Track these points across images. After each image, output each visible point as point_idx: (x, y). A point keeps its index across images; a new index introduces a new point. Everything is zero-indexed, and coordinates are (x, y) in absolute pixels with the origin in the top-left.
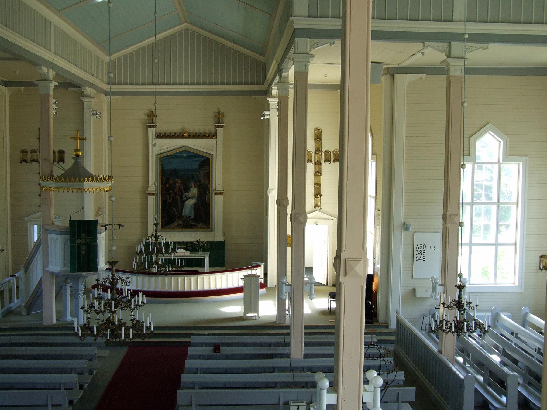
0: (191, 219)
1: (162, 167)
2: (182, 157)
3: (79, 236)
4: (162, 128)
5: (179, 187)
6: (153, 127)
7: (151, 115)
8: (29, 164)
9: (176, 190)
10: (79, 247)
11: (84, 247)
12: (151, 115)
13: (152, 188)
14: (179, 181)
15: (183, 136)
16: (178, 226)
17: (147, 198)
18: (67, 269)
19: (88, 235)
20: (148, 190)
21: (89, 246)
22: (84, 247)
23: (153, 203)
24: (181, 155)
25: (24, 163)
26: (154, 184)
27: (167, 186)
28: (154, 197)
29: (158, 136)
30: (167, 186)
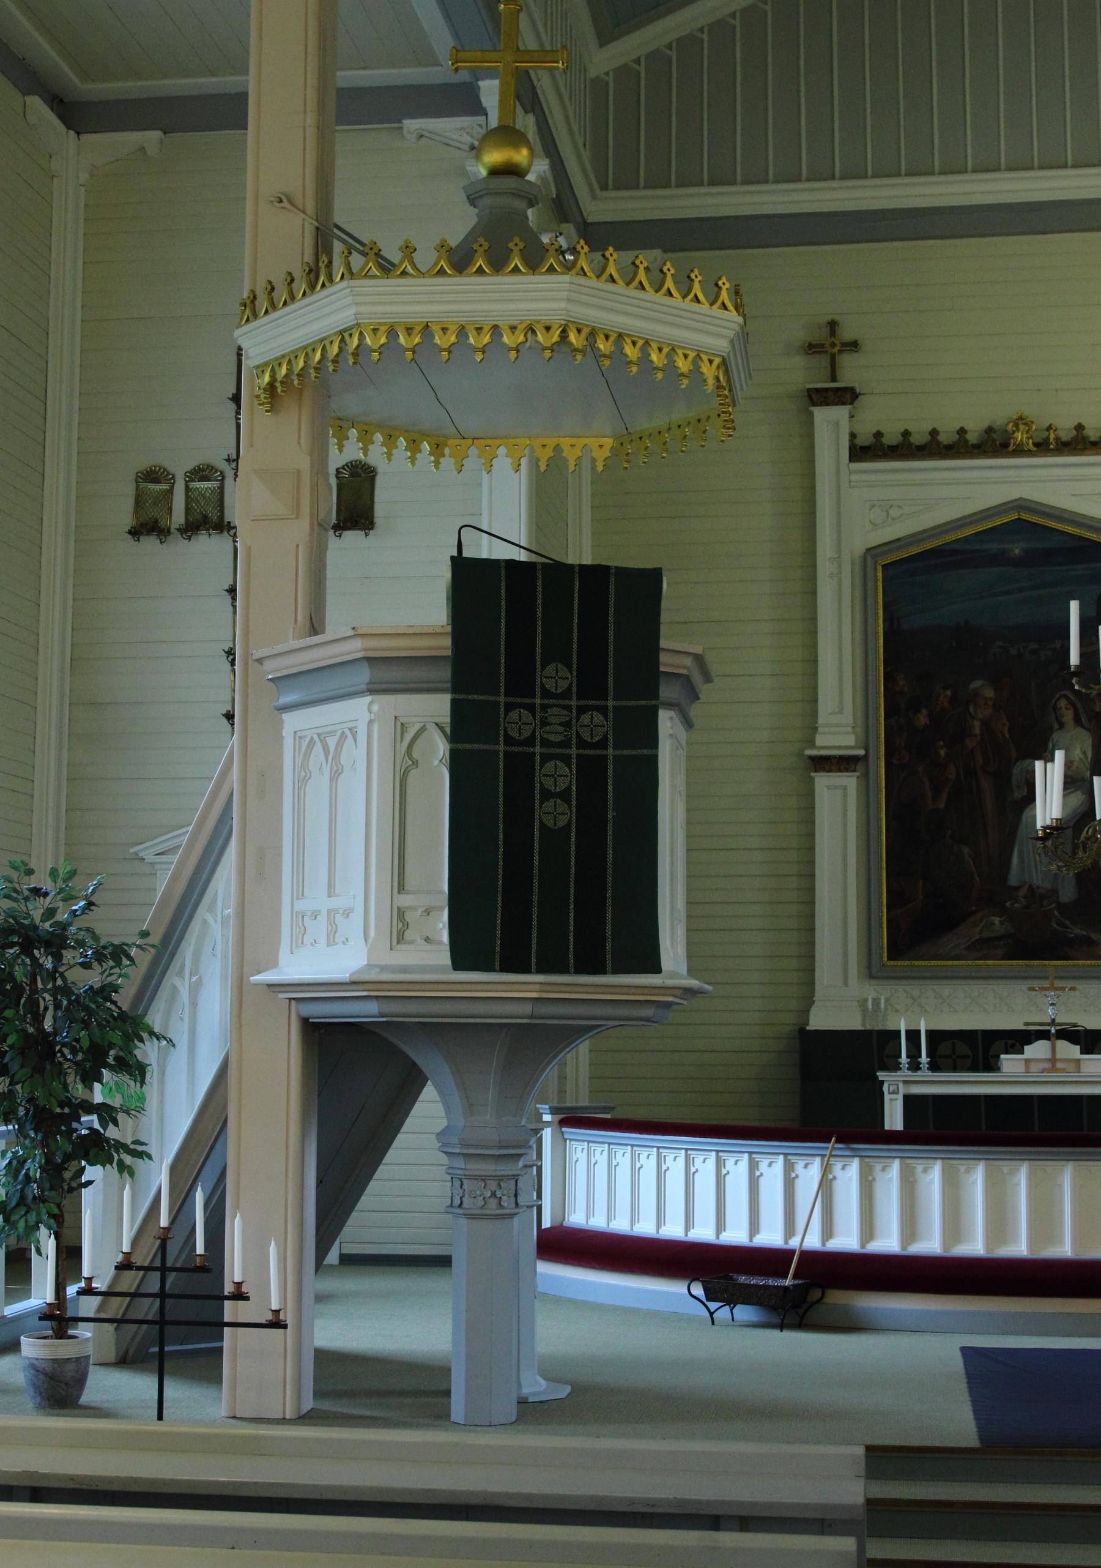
0: (1061, 907)
1: (889, 618)
2: (1000, 559)
3: (521, 683)
4: (883, 416)
5: (986, 724)
6: (846, 396)
7: (829, 344)
8: (179, 546)
9: (970, 743)
10: (520, 768)
11: (557, 775)
12: (829, 344)
13: (838, 732)
14: (989, 693)
15: (1005, 445)
16: (982, 948)
17: (811, 781)
18: (429, 953)
19: (591, 686)
20: (811, 743)
21: (591, 772)
22: (557, 775)
23: (842, 814)
24: (994, 546)
25: (150, 543)
26: (842, 715)
27: (922, 719)
28: (850, 781)
29: (863, 451)
30: (922, 719)
